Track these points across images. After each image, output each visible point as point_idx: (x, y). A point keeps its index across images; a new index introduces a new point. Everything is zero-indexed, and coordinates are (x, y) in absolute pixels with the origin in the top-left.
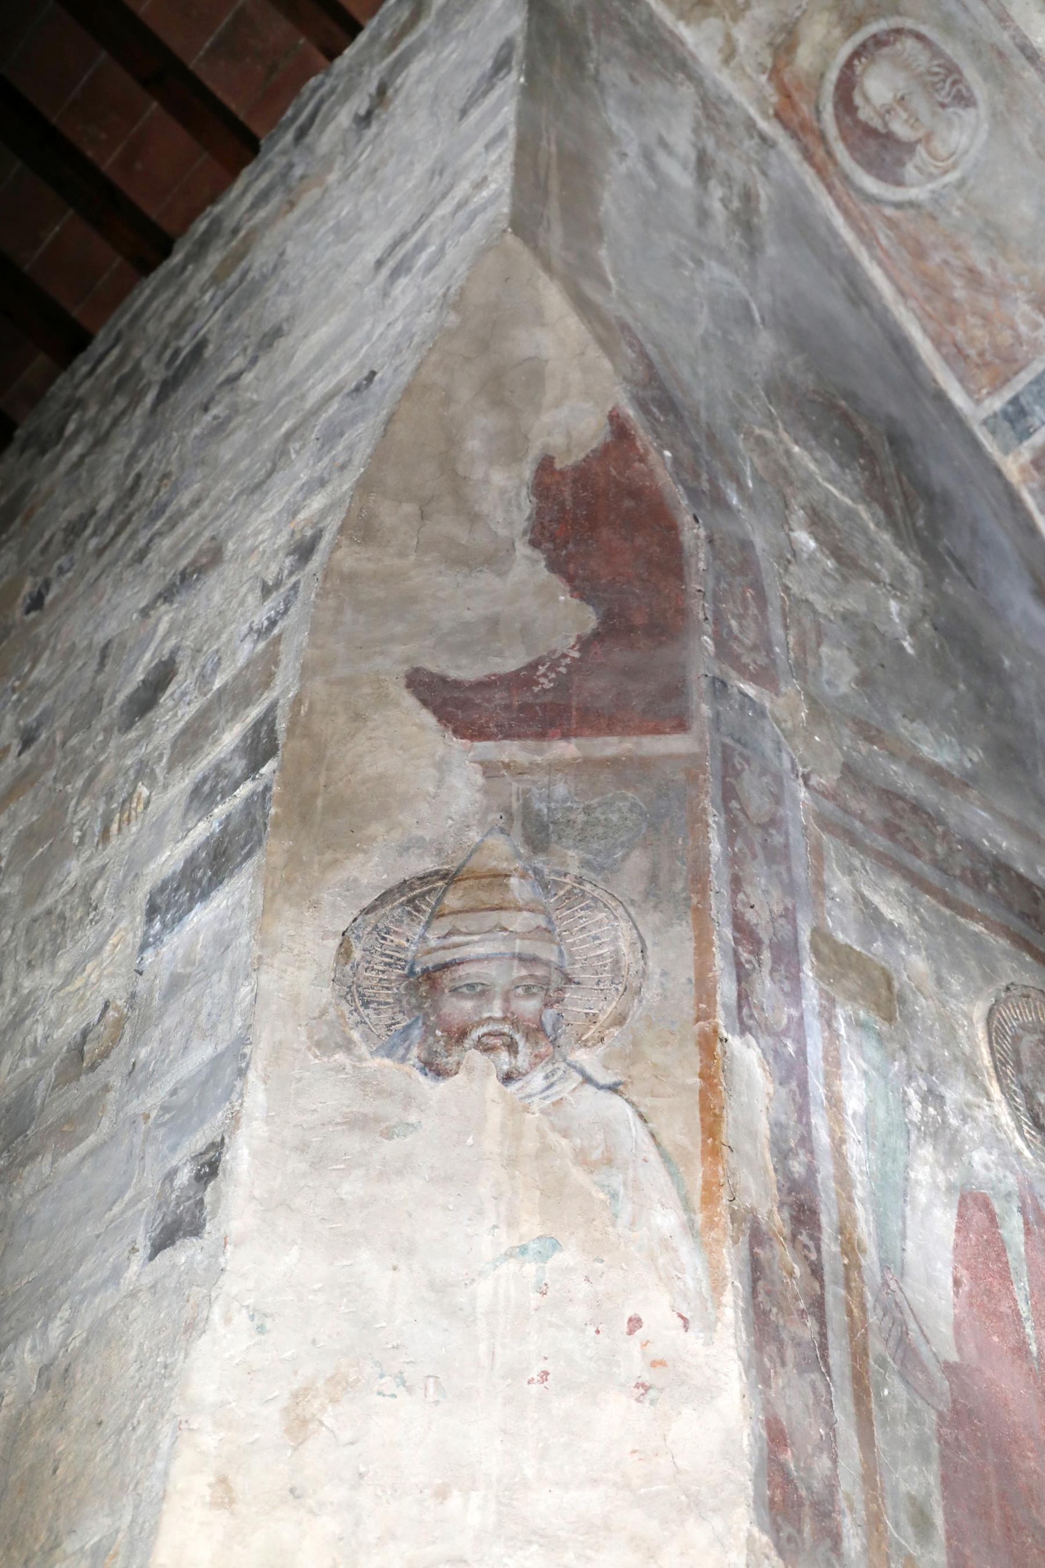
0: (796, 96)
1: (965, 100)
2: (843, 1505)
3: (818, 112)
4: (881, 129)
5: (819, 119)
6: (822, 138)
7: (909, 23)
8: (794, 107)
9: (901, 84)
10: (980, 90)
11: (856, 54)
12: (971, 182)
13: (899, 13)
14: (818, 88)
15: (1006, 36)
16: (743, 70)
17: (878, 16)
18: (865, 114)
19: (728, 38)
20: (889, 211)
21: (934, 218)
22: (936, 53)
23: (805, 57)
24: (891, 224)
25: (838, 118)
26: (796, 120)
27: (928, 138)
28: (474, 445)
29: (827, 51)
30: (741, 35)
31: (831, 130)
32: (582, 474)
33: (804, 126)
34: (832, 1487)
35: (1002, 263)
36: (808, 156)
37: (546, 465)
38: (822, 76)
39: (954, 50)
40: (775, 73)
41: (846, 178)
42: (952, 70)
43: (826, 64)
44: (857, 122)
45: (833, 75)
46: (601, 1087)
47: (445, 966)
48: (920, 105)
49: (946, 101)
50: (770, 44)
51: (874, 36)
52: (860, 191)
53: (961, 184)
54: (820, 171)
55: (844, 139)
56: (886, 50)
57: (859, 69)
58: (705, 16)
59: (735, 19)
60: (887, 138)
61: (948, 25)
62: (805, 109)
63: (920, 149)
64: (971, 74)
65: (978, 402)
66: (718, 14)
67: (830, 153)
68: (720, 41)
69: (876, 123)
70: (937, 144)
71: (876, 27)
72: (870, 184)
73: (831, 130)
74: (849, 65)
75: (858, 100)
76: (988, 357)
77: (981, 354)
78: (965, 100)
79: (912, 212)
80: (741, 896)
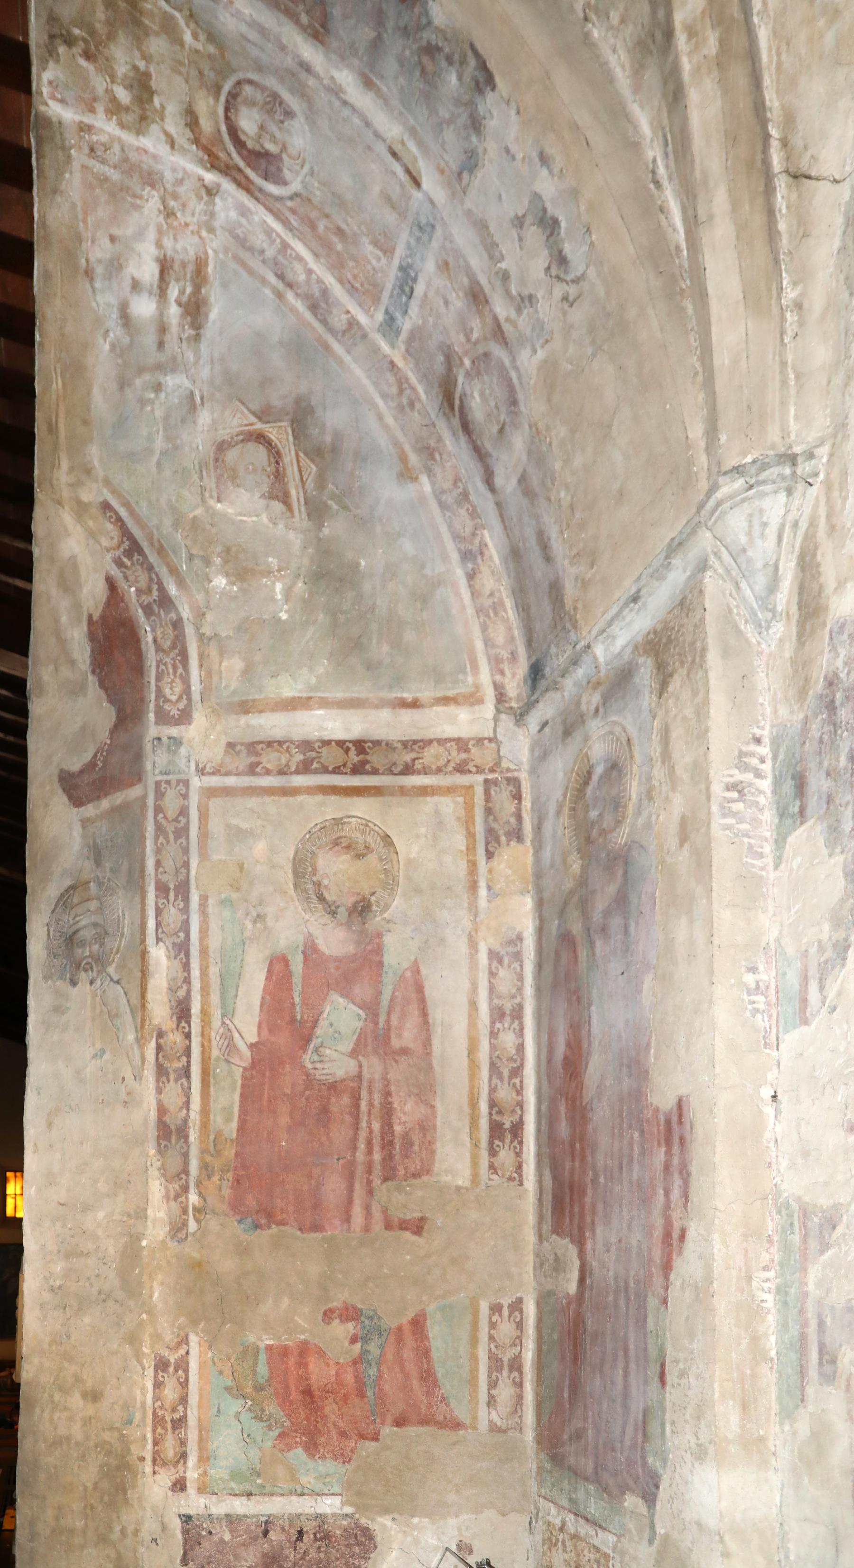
0: (214, 149)
1: (289, 114)
2: (191, 1125)
3: (229, 155)
4: (262, 151)
5: (231, 159)
6: (240, 170)
7: (241, 75)
8: (217, 158)
9: (257, 117)
10: (293, 102)
11: (227, 110)
12: (316, 169)
13: (234, 71)
14: (222, 141)
15: (289, 59)
16: (182, 147)
17: (225, 78)
18: (250, 144)
19: (167, 134)
20: (289, 203)
21: (309, 200)
22: (263, 89)
23: (206, 125)
24: (293, 211)
25: (239, 153)
26: (222, 165)
27: (284, 148)
28: (64, 619)
29: (214, 113)
30: (172, 130)
31: (241, 164)
32: (103, 617)
33: (227, 166)
34: (186, 1121)
35: (350, 220)
36: (239, 184)
37: (90, 617)
38: (219, 131)
39: (271, 82)
40: (196, 141)
41: (261, 190)
42: (275, 96)
43: (217, 123)
44: (249, 151)
45: (223, 128)
46: (384, 140)
47: (75, 933)
48: (273, 128)
49: (282, 118)
50: (186, 125)
51: (229, 93)
52: (270, 195)
53: (312, 173)
54: (248, 191)
55: (249, 166)
56: (239, 99)
57: (233, 117)
58: (148, 126)
59: (162, 120)
60: (265, 155)
61: (259, 68)
62: (222, 155)
63: (284, 156)
64: (286, 95)
65: (372, 317)
66: (153, 121)
67: (247, 178)
68: (163, 137)
69: (258, 148)
70: (290, 150)
71: (227, 87)
72: (272, 189)
73: (241, 164)
74: (227, 118)
75: (243, 137)
76: (366, 286)
77: (362, 285)
78: (289, 114)
79: (298, 200)
80: (161, 869)
